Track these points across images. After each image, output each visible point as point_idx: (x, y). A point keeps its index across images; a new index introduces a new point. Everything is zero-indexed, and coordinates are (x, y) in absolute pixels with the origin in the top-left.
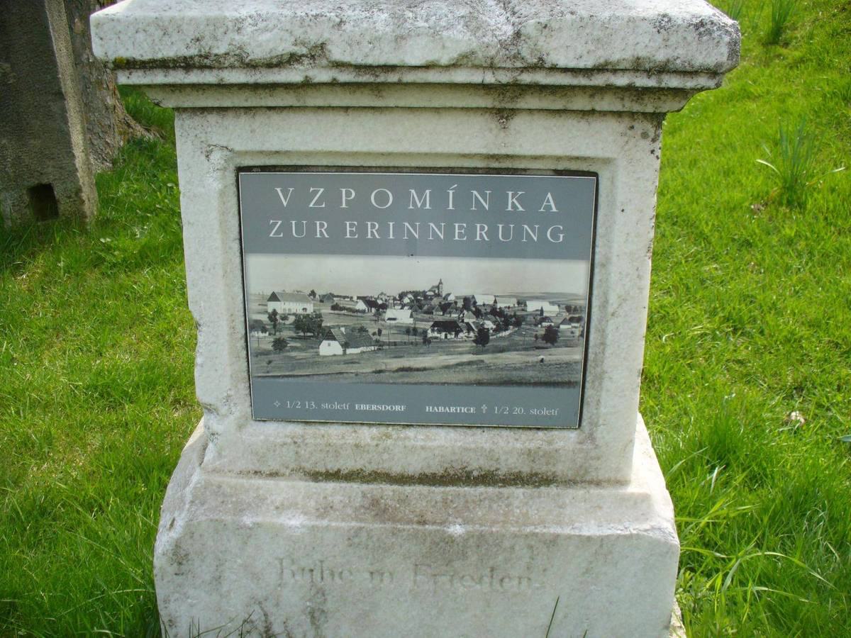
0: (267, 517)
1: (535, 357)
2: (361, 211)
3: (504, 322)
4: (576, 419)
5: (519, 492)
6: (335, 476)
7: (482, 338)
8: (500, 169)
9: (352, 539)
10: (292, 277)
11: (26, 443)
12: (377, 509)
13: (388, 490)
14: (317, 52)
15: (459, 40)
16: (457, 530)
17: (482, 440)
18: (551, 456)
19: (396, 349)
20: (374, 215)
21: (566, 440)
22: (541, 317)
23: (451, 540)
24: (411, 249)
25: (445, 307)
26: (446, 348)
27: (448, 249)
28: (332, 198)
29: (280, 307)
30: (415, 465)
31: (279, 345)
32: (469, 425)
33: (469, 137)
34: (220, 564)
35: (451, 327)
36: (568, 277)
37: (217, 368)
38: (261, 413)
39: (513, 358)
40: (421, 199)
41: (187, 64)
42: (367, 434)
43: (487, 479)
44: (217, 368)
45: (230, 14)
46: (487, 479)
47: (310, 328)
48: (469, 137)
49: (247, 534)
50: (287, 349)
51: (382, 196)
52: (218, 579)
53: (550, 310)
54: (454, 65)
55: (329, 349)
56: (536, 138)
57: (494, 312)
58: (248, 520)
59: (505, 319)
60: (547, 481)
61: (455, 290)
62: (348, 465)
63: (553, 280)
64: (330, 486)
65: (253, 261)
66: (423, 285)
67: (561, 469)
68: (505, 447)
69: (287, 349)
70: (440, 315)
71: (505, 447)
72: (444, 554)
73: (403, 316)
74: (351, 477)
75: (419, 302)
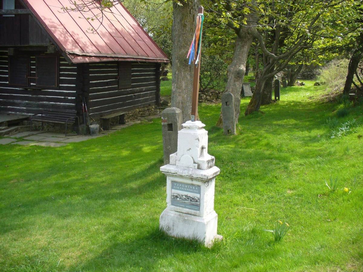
0: (170, 214)
1: (195, 203)
2: (181, 187)
3: (193, 199)
4: (199, 210)
5: (193, 216)
6: (177, 212)
7: (191, 200)
8: (192, 185)
9: (177, 217)
10: (176, 192)
11: (156, 212)
12: (180, 215)
13: (181, 214)
14: (177, 173)
15: (187, 174)
16: (186, 218)
17: (190, 210)
18: (196, 213)
19: (184, 200)
20: (182, 187)
21: (198, 212)
22: (196, 199)
23: (185, 219)
24: (186, 191)
25: (188, 197)
26: (188, 201)
27: (188, 191)
28: (177, 185)
29: (174, 194)
30: (184, 212)
31: (174, 198)
32: (190, 209)
33: (189, 182)
34: (165, 219)
35: (188, 199)
36: (198, 195)
37: (168, 199)
38: (172, 204)
39: (193, 203)
40: (186, 186)
41: (167, 172)
42: (181, 208)
43: (191, 214)
44: (168, 199)
45: (170, 169)
46: (191, 214)
47: (177, 197)
48: (189, 182)
49: (168, 215)
50: (175, 198)
51: (183, 186)
52: (165, 220)
53: (197, 198)
54: (187, 176)
55: (178, 199)
56: (195, 183)
57: (192, 198)
58: (168, 214)
59: (193, 199)
60: (196, 216)
61: (189, 195)
62: (179, 211)
63: (176, 192)
64: (177, 212)
65: (173, 190)
66: (186, 194)
67: (197, 215)
68: (193, 211)
69: (175, 198)
70: (188, 197)
71: (193, 211)
72: (185, 221)
73: (184, 197)
74: (179, 212)
75: (186, 196)
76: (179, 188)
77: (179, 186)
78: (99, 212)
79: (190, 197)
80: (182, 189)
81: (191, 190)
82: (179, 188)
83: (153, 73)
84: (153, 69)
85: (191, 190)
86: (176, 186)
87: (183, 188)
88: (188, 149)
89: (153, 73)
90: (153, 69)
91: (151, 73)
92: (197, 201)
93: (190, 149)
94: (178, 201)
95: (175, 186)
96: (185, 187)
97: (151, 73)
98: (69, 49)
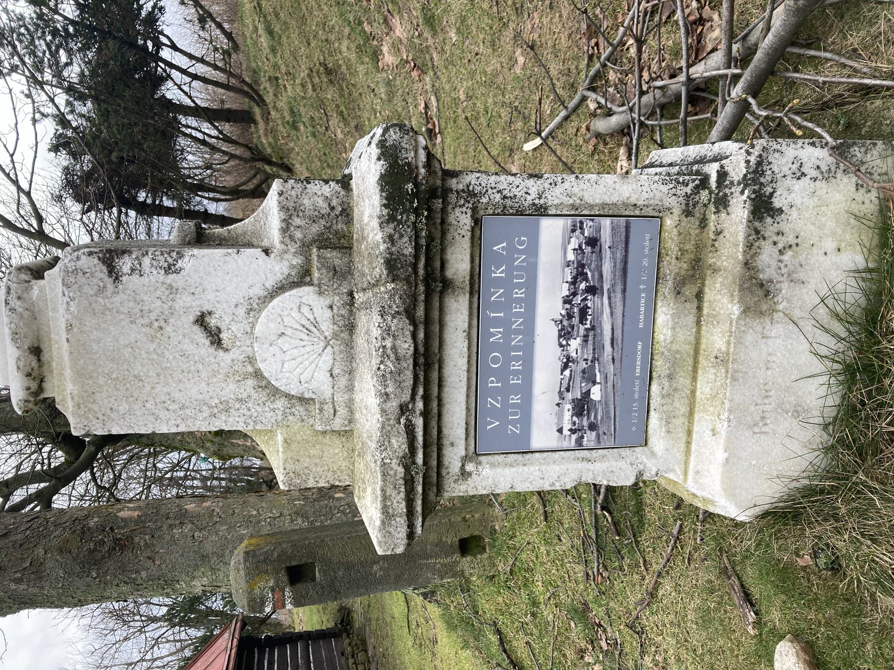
1: (607, 254)
7: (592, 290)
10: (547, 420)
19: (598, 348)
22: (579, 250)
24: (529, 329)
25: (570, 316)
26: (597, 317)
29: (567, 426)
31: (592, 427)
40: (496, 334)
47: (582, 406)
53: (574, 243)
54: (413, 322)
55: (596, 393)
57: (574, 283)
59: (580, 274)
61: (559, 310)
65: (537, 442)
66: (554, 331)
70: (576, 318)
73: (575, 344)
75: (565, 334)
76: (516, 390)
77: (506, 391)
78: (459, 519)
79: (567, 301)
80: (516, 366)
81: (519, 294)
82: (516, 390)
83: (267, 655)
84: (256, 655)
85: (516, 366)
86: (501, 414)
87: (508, 360)
88: (203, 339)
89: (267, 655)
90: (256, 655)
91: (267, 658)
92: (593, 242)
93: (201, 320)
94: (612, 390)
95: (505, 423)
96: (505, 347)
97: (267, 658)
98: (838, 414)
